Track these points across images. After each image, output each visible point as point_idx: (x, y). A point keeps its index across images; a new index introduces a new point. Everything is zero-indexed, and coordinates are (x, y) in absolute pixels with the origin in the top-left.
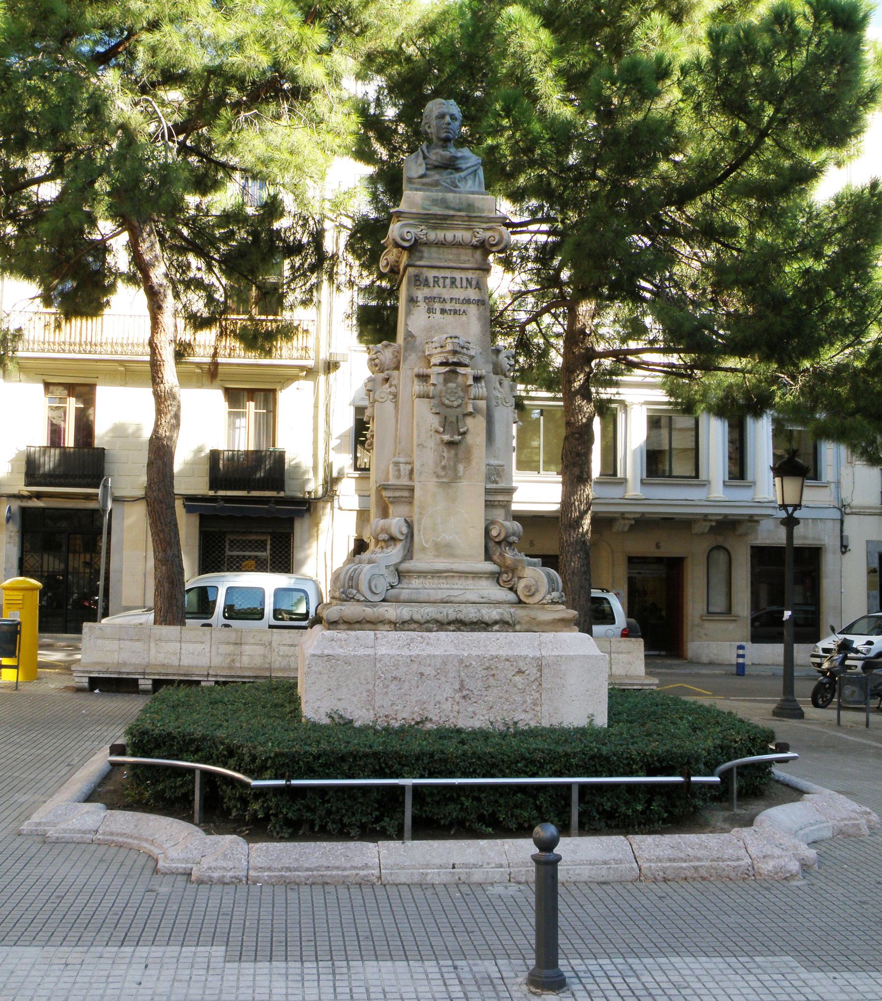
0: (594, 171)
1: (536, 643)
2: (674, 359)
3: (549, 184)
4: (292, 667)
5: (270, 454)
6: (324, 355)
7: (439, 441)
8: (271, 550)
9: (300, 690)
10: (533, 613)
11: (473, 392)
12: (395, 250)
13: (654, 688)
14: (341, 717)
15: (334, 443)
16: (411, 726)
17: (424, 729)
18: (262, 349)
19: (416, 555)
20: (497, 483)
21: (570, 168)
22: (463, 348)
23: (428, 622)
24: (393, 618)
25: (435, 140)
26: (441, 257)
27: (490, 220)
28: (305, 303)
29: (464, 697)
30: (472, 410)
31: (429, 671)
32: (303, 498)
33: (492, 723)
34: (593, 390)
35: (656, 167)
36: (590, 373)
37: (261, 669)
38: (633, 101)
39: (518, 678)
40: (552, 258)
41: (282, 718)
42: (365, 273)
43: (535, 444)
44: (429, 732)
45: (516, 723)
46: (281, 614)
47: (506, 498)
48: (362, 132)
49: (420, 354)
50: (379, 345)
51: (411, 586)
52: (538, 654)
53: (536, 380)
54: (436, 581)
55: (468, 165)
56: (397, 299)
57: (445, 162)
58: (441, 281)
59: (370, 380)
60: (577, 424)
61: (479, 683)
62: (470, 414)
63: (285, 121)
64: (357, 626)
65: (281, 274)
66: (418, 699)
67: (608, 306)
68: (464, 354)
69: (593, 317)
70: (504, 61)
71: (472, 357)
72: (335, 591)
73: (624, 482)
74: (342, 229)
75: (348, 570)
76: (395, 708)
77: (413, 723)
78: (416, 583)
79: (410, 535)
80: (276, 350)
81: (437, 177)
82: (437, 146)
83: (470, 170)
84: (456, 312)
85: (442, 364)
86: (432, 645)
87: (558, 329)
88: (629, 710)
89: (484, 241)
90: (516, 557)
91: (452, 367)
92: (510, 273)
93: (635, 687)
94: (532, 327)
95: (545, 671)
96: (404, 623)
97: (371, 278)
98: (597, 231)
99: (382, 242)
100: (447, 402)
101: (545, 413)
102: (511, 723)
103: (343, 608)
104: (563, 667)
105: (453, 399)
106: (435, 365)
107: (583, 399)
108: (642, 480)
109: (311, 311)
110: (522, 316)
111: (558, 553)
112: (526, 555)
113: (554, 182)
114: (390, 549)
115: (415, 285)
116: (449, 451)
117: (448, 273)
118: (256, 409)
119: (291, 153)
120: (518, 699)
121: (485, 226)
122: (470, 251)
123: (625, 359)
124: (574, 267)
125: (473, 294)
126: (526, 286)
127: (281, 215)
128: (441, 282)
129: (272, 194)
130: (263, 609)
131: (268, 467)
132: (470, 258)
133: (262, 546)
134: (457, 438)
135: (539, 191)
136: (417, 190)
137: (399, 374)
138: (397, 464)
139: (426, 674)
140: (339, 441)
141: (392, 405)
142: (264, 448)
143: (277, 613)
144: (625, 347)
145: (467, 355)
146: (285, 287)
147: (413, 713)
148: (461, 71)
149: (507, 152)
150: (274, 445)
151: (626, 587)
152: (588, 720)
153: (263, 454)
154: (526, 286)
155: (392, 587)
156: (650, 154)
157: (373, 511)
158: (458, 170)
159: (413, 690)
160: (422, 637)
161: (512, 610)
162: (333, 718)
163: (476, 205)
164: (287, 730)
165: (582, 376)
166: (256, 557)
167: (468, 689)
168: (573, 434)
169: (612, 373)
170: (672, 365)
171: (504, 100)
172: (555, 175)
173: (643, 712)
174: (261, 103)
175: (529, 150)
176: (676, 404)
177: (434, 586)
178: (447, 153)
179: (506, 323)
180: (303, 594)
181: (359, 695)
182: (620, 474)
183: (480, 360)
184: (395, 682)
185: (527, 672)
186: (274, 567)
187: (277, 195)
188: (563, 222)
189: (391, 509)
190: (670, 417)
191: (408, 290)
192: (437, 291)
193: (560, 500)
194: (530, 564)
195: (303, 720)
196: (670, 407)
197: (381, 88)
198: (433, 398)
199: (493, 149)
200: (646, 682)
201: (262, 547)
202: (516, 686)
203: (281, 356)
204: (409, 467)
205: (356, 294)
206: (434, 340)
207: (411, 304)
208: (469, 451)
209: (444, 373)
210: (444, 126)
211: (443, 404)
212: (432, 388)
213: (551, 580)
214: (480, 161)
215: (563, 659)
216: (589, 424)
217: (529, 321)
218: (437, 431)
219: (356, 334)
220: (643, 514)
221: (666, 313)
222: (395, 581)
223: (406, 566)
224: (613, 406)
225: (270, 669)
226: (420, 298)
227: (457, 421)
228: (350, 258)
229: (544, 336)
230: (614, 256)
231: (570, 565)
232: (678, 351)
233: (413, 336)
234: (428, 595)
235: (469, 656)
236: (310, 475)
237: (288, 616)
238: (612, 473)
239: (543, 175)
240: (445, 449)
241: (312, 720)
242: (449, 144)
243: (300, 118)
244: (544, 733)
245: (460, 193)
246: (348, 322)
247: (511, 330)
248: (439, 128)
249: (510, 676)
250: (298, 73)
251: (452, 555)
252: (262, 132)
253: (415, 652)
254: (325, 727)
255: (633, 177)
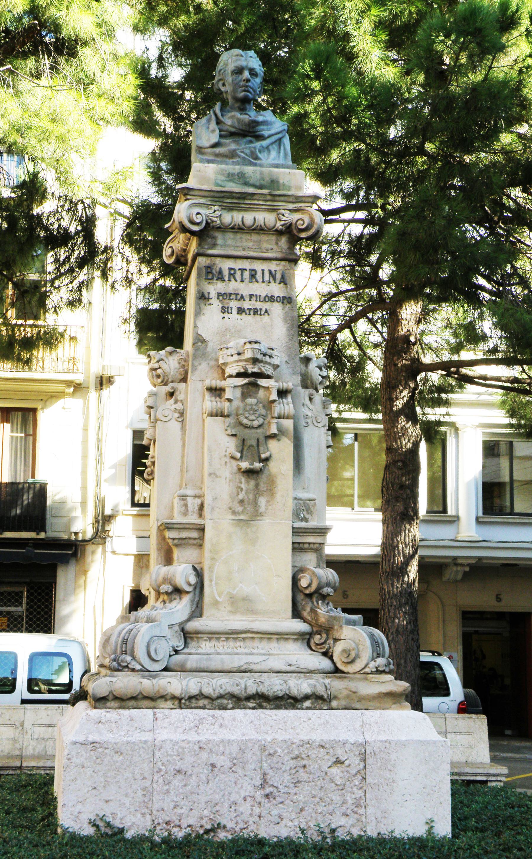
0: (423, 144)
1: (358, 724)
2: (516, 371)
3: (368, 160)
4: (49, 753)
5: (29, 488)
6: (96, 370)
7: (235, 469)
8: (27, 604)
9: (58, 788)
10: (353, 685)
11: (277, 409)
12: (182, 236)
13: (503, 779)
14: (108, 825)
15: (107, 473)
16: (198, 836)
17: (216, 839)
18: (19, 359)
19: (207, 610)
20: (307, 521)
21: (393, 142)
22: (265, 355)
23: (221, 697)
24: (177, 693)
25: (231, 101)
26: (239, 244)
27: (298, 199)
28: (71, 304)
29: (267, 796)
30: (276, 432)
31: (222, 761)
32: (69, 540)
33: (303, 831)
34: (418, 409)
35: (498, 139)
36: (415, 389)
37: (8, 757)
38: (470, 57)
39: (335, 771)
40: (369, 252)
41: (31, 828)
42: (145, 269)
43: (347, 474)
44: (222, 845)
45: (333, 831)
46: (37, 685)
47: (318, 540)
48: (142, 96)
49: (212, 363)
50: (163, 352)
51: (200, 651)
52: (361, 740)
53: (350, 398)
54: (231, 643)
55: (272, 131)
56: (184, 302)
57: (244, 128)
58: (238, 274)
59: (152, 395)
60: (400, 451)
61: (287, 777)
62: (273, 436)
63: (45, 81)
64: (132, 703)
65: (43, 271)
66: (207, 799)
67: (434, 310)
68: (266, 363)
69: (419, 322)
70: (312, 10)
71: (276, 367)
72: (105, 658)
73: (455, 520)
74: (118, 217)
75: (121, 631)
76: (179, 811)
77: (201, 832)
78: (206, 646)
79: (200, 586)
80: (38, 361)
81: (233, 146)
82: (233, 109)
83: (273, 139)
84: (256, 312)
85: (239, 375)
86: (226, 727)
87: (376, 338)
88: (478, 813)
89: (291, 224)
90: (332, 614)
91: (251, 379)
92: (319, 270)
93: (479, 778)
94: (344, 336)
95: (370, 761)
96: (191, 698)
97: (152, 275)
98: (425, 218)
99: (166, 226)
100: (245, 421)
101: (359, 439)
102: (327, 830)
103: (114, 679)
104: (393, 756)
105: (252, 417)
106: (231, 376)
107: (408, 420)
108: (477, 518)
109: (79, 312)
110: (333, 323)
111: (377, 606)
112: (344, 611)
113: (374, 159)
114: (174, 603)
115: (207, 279)
116: (247, 482)
117: (246, 264)
118: (12, 431)
119: (54, 120)
120: (336, 798)
121: (291, 206)
122: (273, 238)
123: (457, 372)
124: (395, 263)
125: (277, 290)
126: (337, 287)
127: (44, 197)
128: (238, 275)
129: (31, 171)
130: (15, 680)
131: (26, 502)
132: (275, 247)
133: (16, 600)
134: (258, 465)
135: (355, 169)
136: (209, 161)
137: (187, 387)
138: (183, 497)
139: (218, 766)
140: (113, 471)
141: (179, 425)
142: (20, 479)
143: (32, 684)
144: (455, 358)
145: (270, 364)
146: (48, 285)
147: (202, 818)
148: (261, 23)
149: (317, 122)
150: (33, 476)
151: (460, 648)
152: (427, 827)
153: (20, 486)
154: (337, 287)
155: (177, 652)
156: (489, 123)
157: (154, 555)
158: (260, 138)
159: (201, 787)
160: (213, 716)
161: (327, 681)
162: (97, 826)
163: (281, 181)
164: (36, 846)
165: (405, 393)
166: (9, 613)
167: (272, 785)
168: (395, 462)
169: (441, 389)
170: (516, 380)
171: (314, 58)
172: (375, 149)
173: (497, 816)
174: (16, 57)
175: (343, 120)
176: (519, 426)
177: (229, 650)
178: (246, 117)
179: (315, 331)
180: (65, 660)
181: (132, 795)
182: (451, 511)
183: (285, 370)
184: (180, 777)
185: (347, 763)
186: (31, 626)
187: (38, 173)
188: (383, 207)
189: (176, 553)
190: (511, 443)
191: (198, 284)
192: (232, 286)
193: (380, 542)
194: (349, 623)
195: (59, 830)
196: (512, 431)
197: (164, 44)
198: (228, 416)
199: (301, 118)
200: (493, 771)
201: (17, 601)
202: (332, 781)
203: (43, 368)
204: (198, 501)
205: (134, 293)
206: (229, 346)
207: (202, 302)
208: (272, 482)
209: (242, 386)
210: (242, 83)
211: (241, 424)
212: (227, 404)
213: (375, 643)
214: (286, 127)
215: (393, 745)
216: (414, 451)
217: (341, 329)
218: (233, 458)
219: (134, 342)
220: (480, 559)
221: (512, 315)
222: (180, 644)
223: (192, 626)
224: (443, 429)
225: (21, 757)
226: (213, 295)
227: (258, 445)
228: (128, 250)
229: (360, 346)
230: (445, 247)
231: (393, 622)
232: (520, 363)
233: (203, 341)
234: (222, 662)
235: (273, 741)
236: (78, 513)
237: (47, 688)
238: (441, 509)
239: (360, 150)
240: (243, 480)
241: (71, 830)
242: (248, 106)
243: (65, 77)
244: (371, 845)
245: (261, 166)
246: (126, 327)
247: (319, 338)
248: (236, 85)
249: (325, 768)
250: (61, 21)
251: (253, 612)
252: (18, 93)
253: (204, 737)
254: (87, 839)
255: (470, 153)
